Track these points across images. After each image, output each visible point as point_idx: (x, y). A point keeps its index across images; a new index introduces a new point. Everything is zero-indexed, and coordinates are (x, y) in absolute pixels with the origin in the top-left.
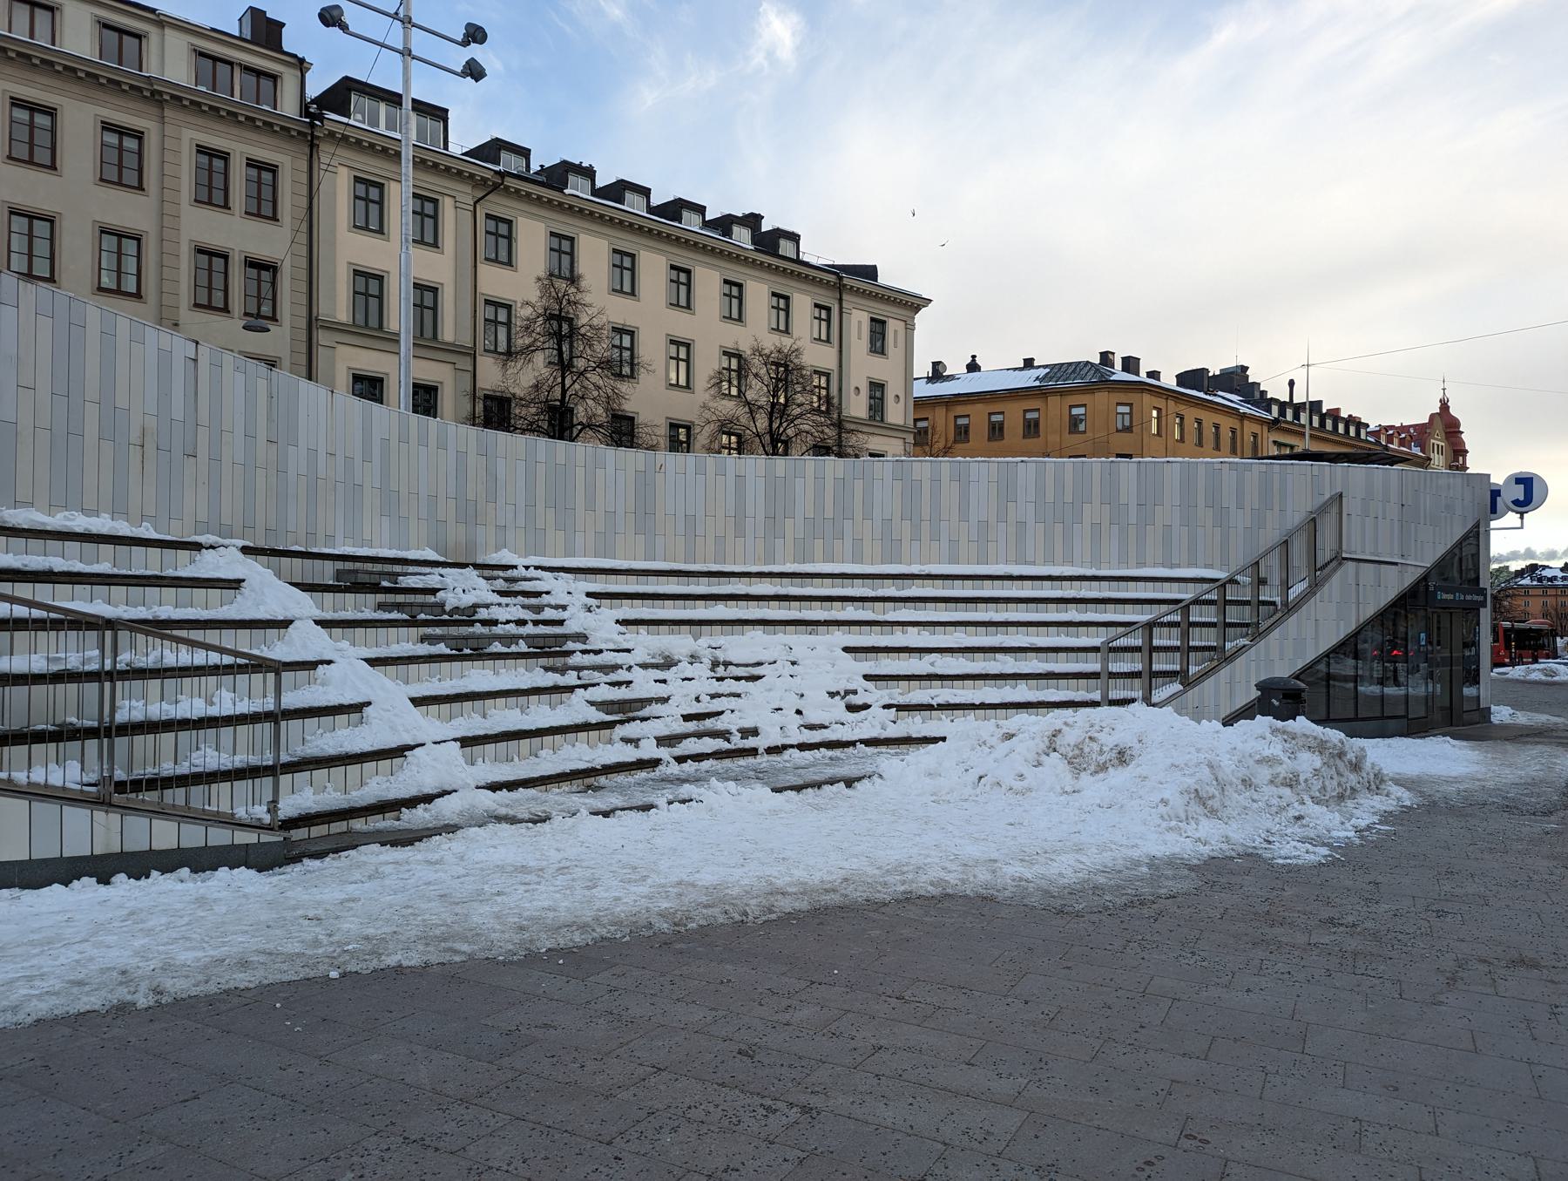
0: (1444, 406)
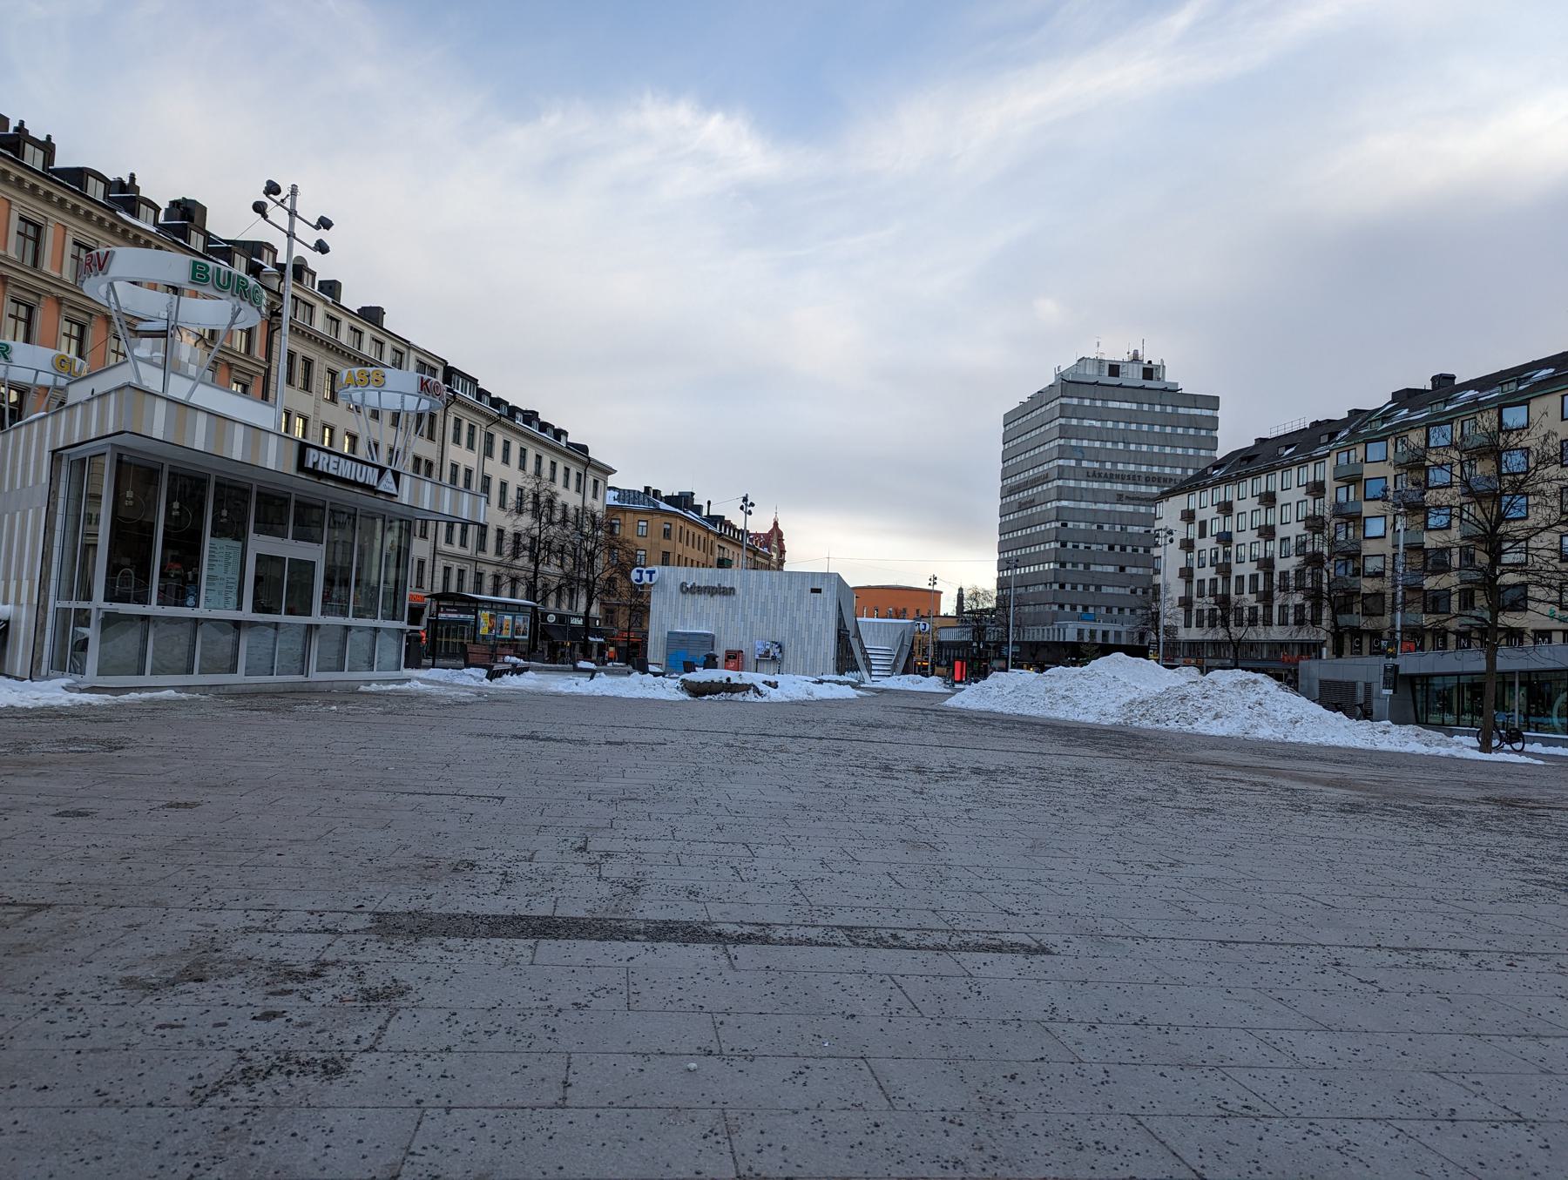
0: (776, 524)
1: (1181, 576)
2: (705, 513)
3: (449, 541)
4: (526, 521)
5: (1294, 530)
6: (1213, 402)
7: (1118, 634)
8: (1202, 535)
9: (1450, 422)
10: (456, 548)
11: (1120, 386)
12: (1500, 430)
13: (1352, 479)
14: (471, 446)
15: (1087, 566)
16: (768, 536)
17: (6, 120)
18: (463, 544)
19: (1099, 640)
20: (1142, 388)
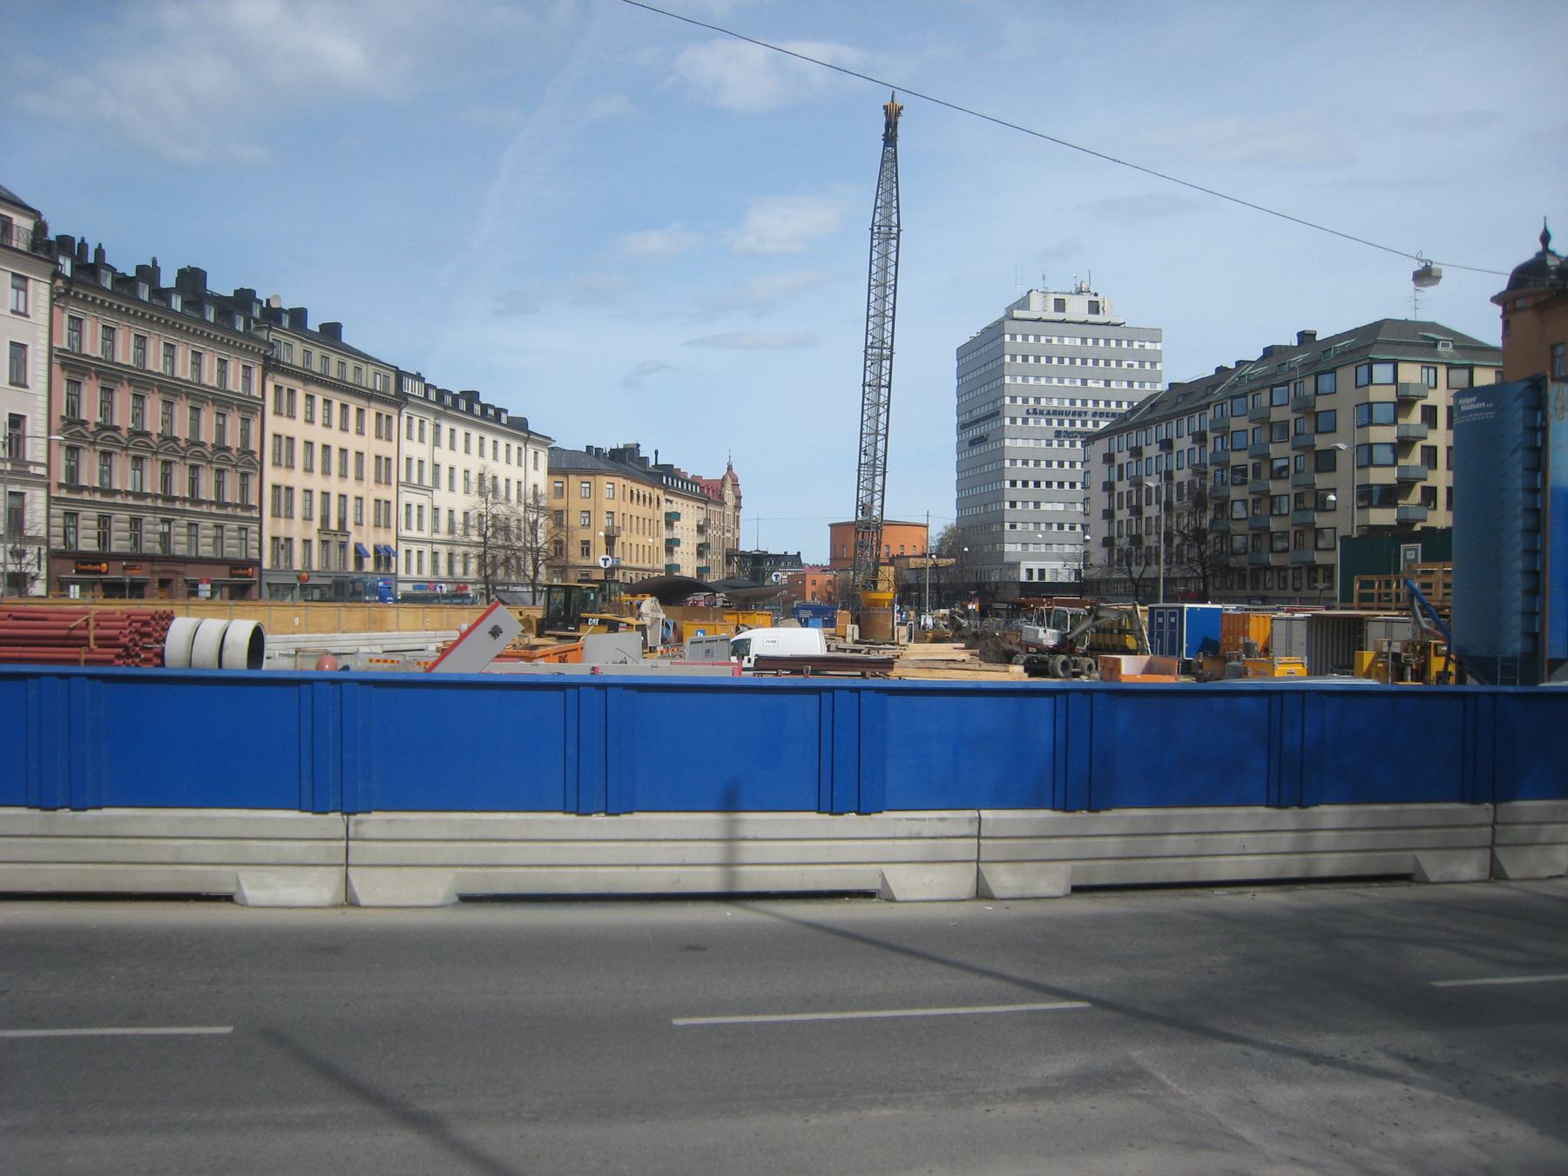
0: (730, 468)
1: (1104, 517)
2: (652, 463)
3: (408, 527)
4: (474, 499)
5: (1183, 475)
6: (1155, 335)
7: (1056, 571)
8: (1120, 478)
9: (1287, 383)
10: (414, 533)
11: (1063, 321)
12: (1317, 393)
13: (1224, 431)
14: (421, 440)
15: (1037, 504)
16: (723, 481)
17: (73, 239)
18: (420, 529)
19: (1036, 579)
20: (1086, 323)
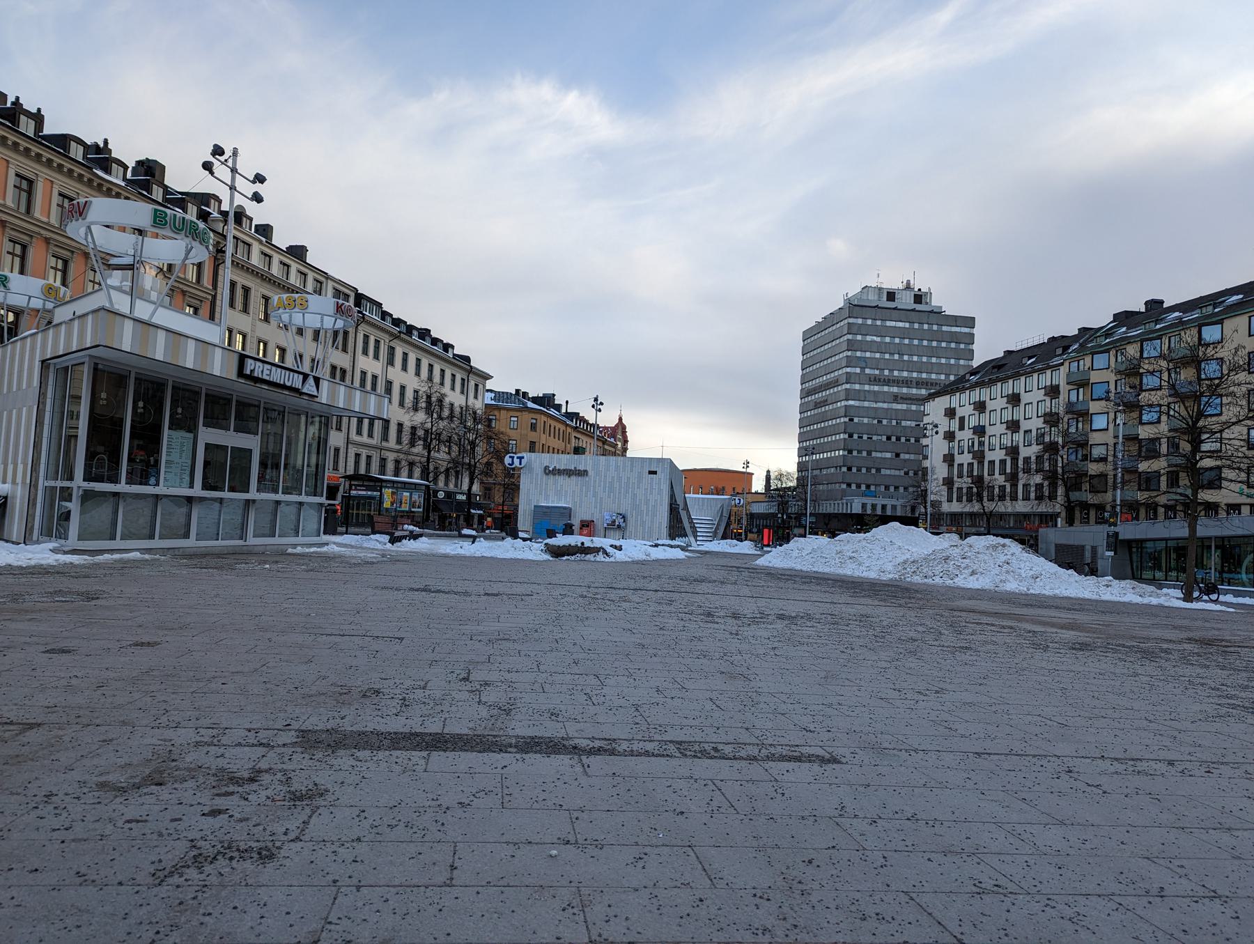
0: (620, 419)
1: (944, 461)
2: (564, 410)
3: (359, 432)
4: (420, 417)
5: (1035, 424)
6: (970, 322)
7: (894, 507)
8: (962, 428)
9: (1160, 337)
10: (364, 438)
11: (895, 309)
12: (1200, 344)
13: (1081, 383)
14: (376, 357)
15: (869, 453)
16: (614, 429)
17: (5, 96)
18: (370, 435)
19: (879, 512)
20: (913, 310)
